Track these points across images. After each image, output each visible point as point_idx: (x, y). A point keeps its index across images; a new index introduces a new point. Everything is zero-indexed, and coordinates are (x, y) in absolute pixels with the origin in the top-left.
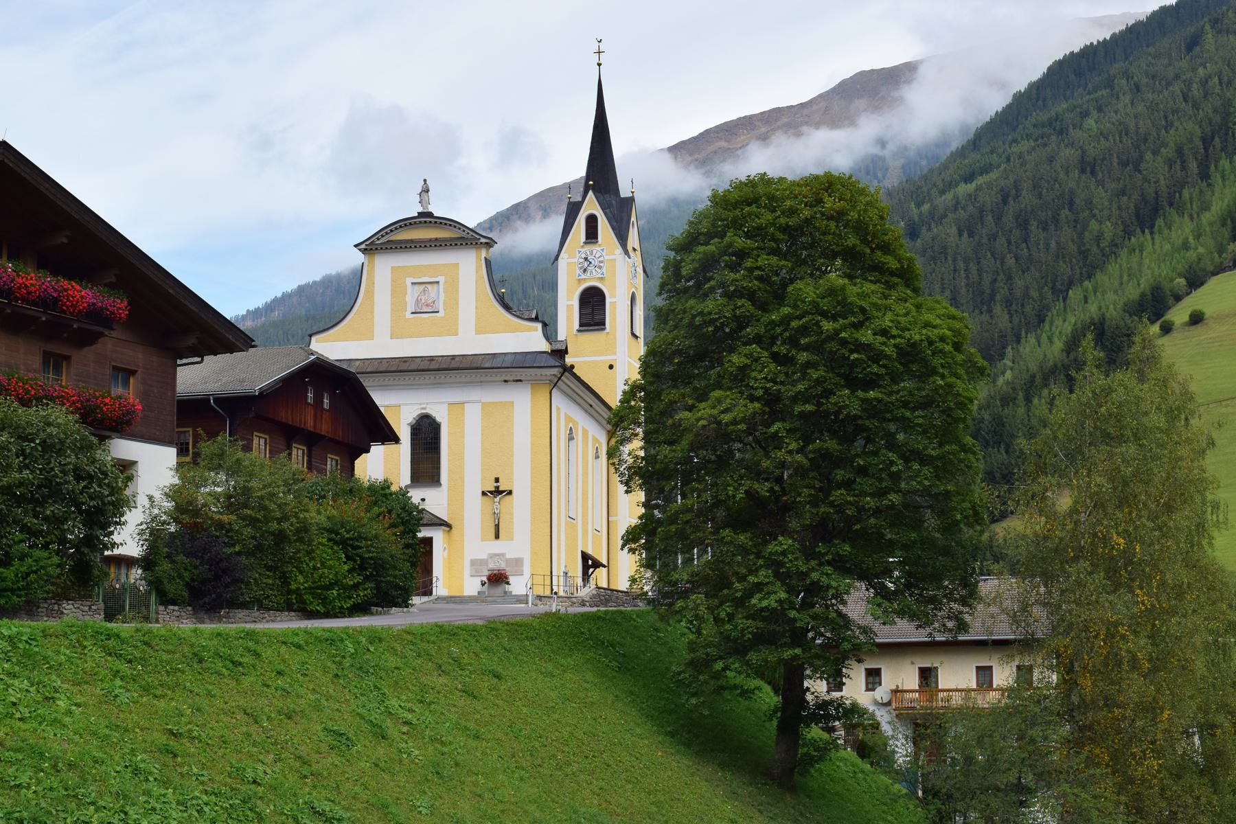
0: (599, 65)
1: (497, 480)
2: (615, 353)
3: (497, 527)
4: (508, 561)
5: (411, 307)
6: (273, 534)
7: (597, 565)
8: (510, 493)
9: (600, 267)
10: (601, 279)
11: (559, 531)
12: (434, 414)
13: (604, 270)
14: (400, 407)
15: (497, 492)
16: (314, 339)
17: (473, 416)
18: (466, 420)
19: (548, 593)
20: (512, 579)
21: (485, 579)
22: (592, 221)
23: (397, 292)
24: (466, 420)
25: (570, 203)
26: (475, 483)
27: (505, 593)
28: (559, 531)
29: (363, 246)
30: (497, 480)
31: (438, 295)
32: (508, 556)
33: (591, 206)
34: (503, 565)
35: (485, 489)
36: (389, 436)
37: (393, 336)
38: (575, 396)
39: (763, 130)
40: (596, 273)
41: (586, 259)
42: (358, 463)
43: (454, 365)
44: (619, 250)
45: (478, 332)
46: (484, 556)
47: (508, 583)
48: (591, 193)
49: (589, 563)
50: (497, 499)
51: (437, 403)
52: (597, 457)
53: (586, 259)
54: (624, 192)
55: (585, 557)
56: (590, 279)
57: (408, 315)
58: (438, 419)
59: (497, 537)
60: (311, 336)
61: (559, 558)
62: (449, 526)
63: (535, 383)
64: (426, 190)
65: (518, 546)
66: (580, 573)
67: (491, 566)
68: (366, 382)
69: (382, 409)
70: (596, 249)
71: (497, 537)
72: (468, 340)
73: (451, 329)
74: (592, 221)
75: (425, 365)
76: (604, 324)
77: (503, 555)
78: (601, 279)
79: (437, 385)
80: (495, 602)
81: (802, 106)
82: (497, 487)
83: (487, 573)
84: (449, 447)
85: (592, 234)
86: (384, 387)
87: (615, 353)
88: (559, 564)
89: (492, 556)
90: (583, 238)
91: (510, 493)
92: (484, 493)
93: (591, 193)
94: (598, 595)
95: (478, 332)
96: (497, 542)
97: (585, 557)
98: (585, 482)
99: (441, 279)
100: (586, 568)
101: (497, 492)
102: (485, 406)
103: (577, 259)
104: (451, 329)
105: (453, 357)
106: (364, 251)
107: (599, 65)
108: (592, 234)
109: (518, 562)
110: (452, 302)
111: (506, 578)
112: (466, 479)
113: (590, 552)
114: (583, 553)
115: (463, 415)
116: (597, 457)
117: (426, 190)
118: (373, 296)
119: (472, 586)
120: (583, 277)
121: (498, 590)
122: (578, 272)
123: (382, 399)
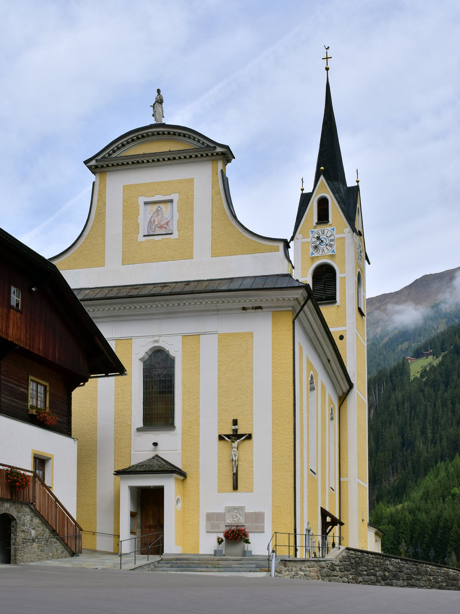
0: (327, 69)
1: (235, 422)
2: (345, 325)
3: (235, 476)
4: (248, 516)
5: (143, 230)
7: (336, 522)
8: (249, 437)
9: (331, 246)
10: (332, 256)
11: (302, 484)
12: (167, 347)
13: (334, 248)
14: (131, 341)
15: (235, 436)
17: (209, 348)
18: (202, 353)
19: (292, 558)
20: (252, 537)
21: (222, 536)
22: (323, 203)
23: (130, 213)
24: (202, 353)
25: (302, 195)
26: (211, 426)
27: (244, 553)
28: (302, 484)
29: (93, 163)
30: (235, 422)
32: (247, 510)
34: (241, 521)
36: (110, 365)
37: (127, 260)
38: (316, 342)
39: (378, 305)
40: (327, 251)
41: (318, 238)
42: (78, 394)
43: (188, 289)
44: (348, 229)
45: (214, 255)
46: (220, 510)
47: (247, 542)
48: (322, 178)
49: (329, 521)
50: (235, 444)
51: (170, 336)
52: (332, 419)
53: (318, 238)
54: (350, 183)
55: (324, 514)
56: (322, 257)
57: (140, 238)
58: (172, 353)
59: (235, 488)
61: (302, 515)
62: (183, 474)
63: (276, 311)
64: (160, 101)
65: (258, 499)
66: (320, 533)
67: (229, 521)
68: (92, 311)
69: (112, 344)
70: (327, 228)
71: (235, 488)
73: (185, 252)
75: (157, 290)
76: (335, 299)
77: (242, 508)
78: (332, 256)
79: (170, 315)
80: (228, 568)
81: (397, 293)
82: (236, 431)
83: (224, 529)
84: (184, 385)
85: (323, 217)
86: (115, 318)
87: (345, 325)
88: (302, 520)
89: (230, 509)
90: (315, 220)
92: (221, 438)
93: (322, 178)
94: (349, 557)
95: (214, 255)
96: (235, 494)
97: (324, 514)
98: (323, 438)
99: (175, 197)
100: (325, 525)
101: (235, 436)
102: (222, 337)
103: (311, 239)
104: (185, 252)
105: (188, 283)
106: (94, 170)
107: (327, 69)
108: (323, 217)
109: (258, 517)
110: (187, 222)
111: (246, 535)
112: (202, 421)
113: (327, 509)
114: (321, 508)
115: (199, 348)
116: (332, 419)
117: (160, 101)
118: (104, 218)
119: (208, 544)
120: (316, 255)
121: (237, 549)
122: (311, 250)
123: (110, 332)
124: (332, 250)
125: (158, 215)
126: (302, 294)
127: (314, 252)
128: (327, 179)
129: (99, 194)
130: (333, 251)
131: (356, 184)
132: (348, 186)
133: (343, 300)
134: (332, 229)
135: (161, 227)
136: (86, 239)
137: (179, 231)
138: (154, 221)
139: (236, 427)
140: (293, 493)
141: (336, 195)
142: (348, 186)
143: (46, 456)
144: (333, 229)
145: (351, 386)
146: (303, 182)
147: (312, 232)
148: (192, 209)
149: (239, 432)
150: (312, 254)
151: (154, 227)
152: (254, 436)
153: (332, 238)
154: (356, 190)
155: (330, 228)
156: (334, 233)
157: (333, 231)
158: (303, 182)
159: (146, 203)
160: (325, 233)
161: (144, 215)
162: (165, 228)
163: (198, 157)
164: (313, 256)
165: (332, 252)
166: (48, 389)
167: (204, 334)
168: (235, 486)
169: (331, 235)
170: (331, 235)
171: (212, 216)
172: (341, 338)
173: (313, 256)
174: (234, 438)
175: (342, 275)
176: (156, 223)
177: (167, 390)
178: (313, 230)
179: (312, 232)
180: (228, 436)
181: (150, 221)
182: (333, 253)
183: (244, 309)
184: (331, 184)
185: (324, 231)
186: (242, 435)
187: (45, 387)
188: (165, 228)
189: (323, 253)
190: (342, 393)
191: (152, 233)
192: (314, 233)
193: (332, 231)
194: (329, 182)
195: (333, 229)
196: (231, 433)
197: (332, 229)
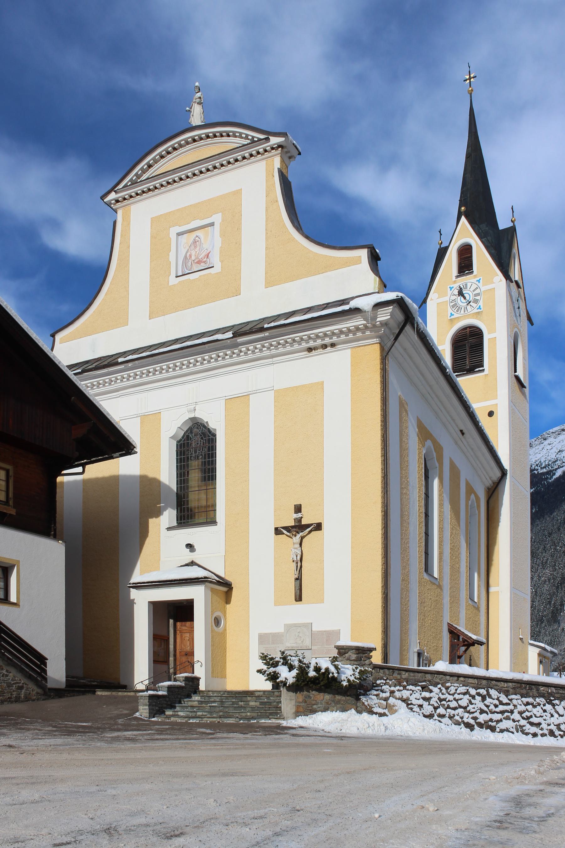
1: (298, 509)
6: (323, 685)
8: (319, 527)
9: (476, 301)
13: (481, 303)
15: (299, 527)
16: (58, 337)
22: (465, 253)
30: (298, 509)
31: (212, 242)
33: (466, 233)
35: (280, 525)
54: (503, 223)
55: (454, 633)
56: (466, 317)
58: (212, 426)
59: (299, 598)
60: (53, 336)
70: (467, 279)
71: (299, 598)
72: (258, 302)
74: (465, 253)
82: (299, 520)
84: (227, 465)
85: (465, 264)
91: (319, 527)
92: (278, 531)
96: (299, 606)
99: (217, 218)
101: (299, 527)
108: (465, 264)
120: (456, 315)
122: (450, 311)
124: (478, 307)
125: (195, 247)
126: (392, 314)
127: (453, 313)
128: (467, 217)
129: (122, 235)
130: (480, 308)
131: (512, 224)
132: (500, 229)
133: (494, 366)
134: (477, 281)
135: (199, 262)
136: (106, 295)
137: (222, 261)
138: (190, 256)
139: (299, 515)
140: (486, 619)
141: (483, 240)
142: (500, 229)
143: (7, 561)
144: (479, 281)
145: (504, 473)
146: (441, 234)
147: (451, 288)
148: (239, 229)
149: (304, 522)
150: (452, 315)
151: (190, 264)
152: (324, 526)
153: (478, 291)
154: (512, 231)
155: (474, 280)
156: (480, 285)
157: (479, 282)
158: (441, 234)
159: (179, 234)
160: (468, 287)
161: (178, 250)
162: (204, 262)
163: (246, 158)
164: (452, 317)
165: (478, 309)
166: (11, 473)
167: (255, 392)
168: (298, 597)
169: (477, 288)
170: (477, 288)
171: (267, 233)
172: (491, 414)
173: (452, 317)
174: (294, 529)
175: (492, 336)
176: (193, 258)
177: (207, 475)
178: (451, 286)
179: (451, 288)
180: (287, 528)
181: (186, 257)
182: (479, 310)
183: (310, 350)
184: (477, 227)
185: (466, 285)
186: (308, 526)
187: (7, 471)
188: (204, 262)
189: (466, 312)
190: (490, 482)
191: (188, 272)
192: (453, 289)
193: (477, 283)
194: (473, 226)
195: (479, 281)
196: (293, 524)
197: (477, 281)
